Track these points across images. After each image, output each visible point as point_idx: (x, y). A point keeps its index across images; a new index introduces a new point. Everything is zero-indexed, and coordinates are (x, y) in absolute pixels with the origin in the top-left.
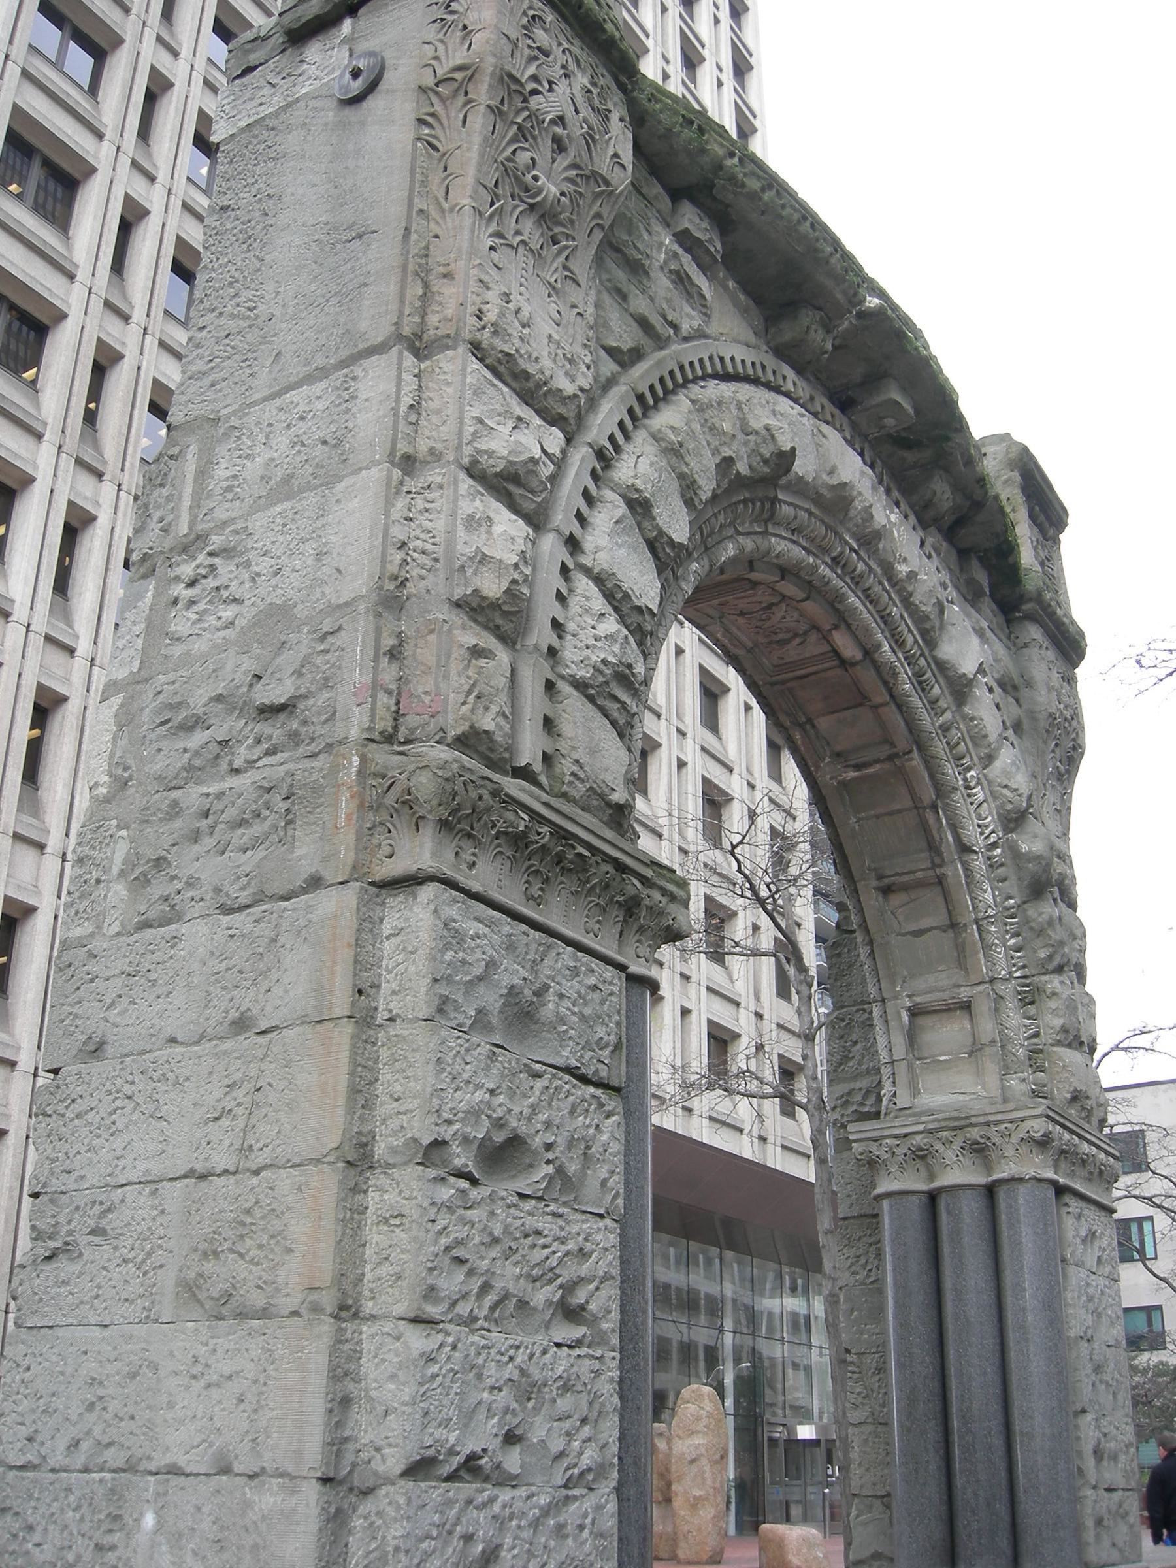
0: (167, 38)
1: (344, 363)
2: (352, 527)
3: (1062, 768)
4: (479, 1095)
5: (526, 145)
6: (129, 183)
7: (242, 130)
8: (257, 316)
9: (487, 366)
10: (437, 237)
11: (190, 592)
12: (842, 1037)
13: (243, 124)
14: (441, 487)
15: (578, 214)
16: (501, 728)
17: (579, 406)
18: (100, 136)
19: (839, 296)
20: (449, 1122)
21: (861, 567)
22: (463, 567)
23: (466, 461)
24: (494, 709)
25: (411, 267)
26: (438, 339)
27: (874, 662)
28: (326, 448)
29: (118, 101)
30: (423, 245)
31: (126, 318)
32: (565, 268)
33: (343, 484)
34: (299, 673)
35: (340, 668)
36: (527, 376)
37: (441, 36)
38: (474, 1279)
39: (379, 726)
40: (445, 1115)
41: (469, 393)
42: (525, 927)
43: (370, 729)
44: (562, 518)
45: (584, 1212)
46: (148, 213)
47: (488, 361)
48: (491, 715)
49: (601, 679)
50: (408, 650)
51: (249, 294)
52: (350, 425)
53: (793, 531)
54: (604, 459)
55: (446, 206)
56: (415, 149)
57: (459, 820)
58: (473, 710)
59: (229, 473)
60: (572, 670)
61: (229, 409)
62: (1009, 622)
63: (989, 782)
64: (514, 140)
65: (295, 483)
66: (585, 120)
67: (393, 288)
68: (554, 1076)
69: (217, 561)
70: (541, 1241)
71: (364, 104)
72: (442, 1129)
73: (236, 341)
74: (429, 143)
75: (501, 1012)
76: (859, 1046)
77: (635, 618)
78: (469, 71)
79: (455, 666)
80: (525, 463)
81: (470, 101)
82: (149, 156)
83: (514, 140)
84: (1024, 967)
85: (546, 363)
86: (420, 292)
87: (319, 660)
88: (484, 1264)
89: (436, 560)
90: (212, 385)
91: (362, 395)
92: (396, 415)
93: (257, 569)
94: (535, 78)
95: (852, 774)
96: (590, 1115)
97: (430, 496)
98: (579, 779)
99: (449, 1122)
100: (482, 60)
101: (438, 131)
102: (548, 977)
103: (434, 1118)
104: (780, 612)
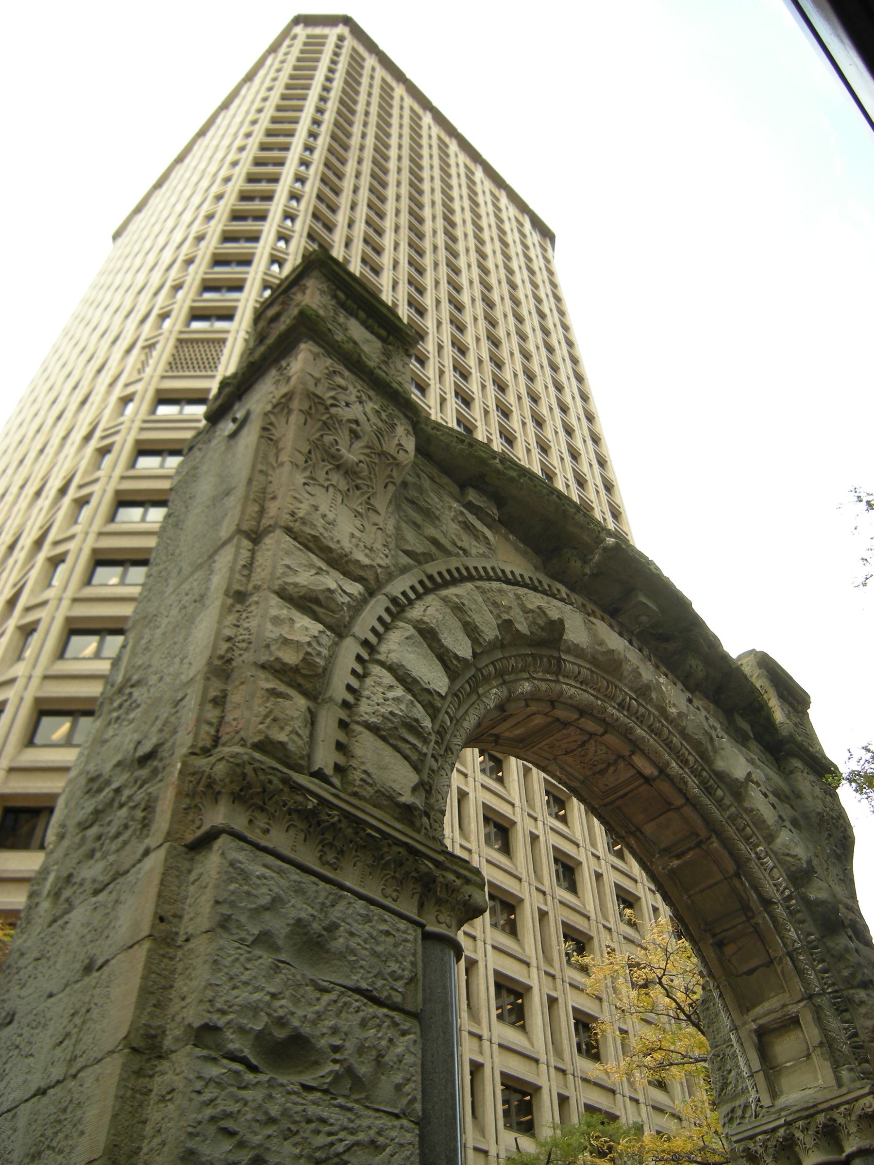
3: (838, 851)
4: (257, 996)
9: (300, 543)
12: (720, 1069)
19: (586, 538)
20: (223, 1012)
21: (642, 710)
27: (668, 776)
32: (367, 503)
36: (330, 550)
38: (245, 1151)
39: (201, 744)
40: (219, 1005)
42: (314, 879)
45: (378, 1110)
53: (581, 683)
57: (249, 792)
58: (268, 727)
62: (777, 760)
63: (775, 853)
68: (342, 993)
70: (327, 1129)
72: (215, 1017)
75: (286, 937)
76: (733, 1073)
77: (426, 697)
79: (257, 701)
80: (323, 591)
84: (833, 984)
88: (257, 1139)
89: (250, 643)
95: (676, 863)
96: (384, 1030)
98: (367, 783)
99: (223, 1012)
102: (339, 918)
103: (207, 1006)
104: (592, 747)
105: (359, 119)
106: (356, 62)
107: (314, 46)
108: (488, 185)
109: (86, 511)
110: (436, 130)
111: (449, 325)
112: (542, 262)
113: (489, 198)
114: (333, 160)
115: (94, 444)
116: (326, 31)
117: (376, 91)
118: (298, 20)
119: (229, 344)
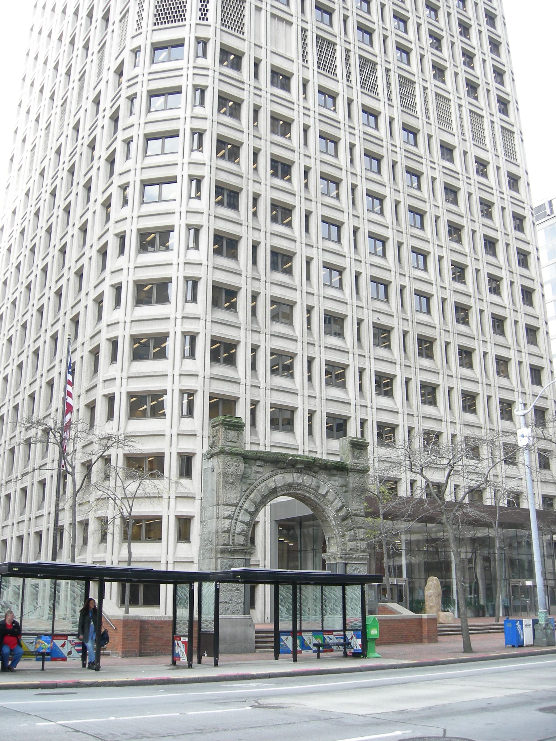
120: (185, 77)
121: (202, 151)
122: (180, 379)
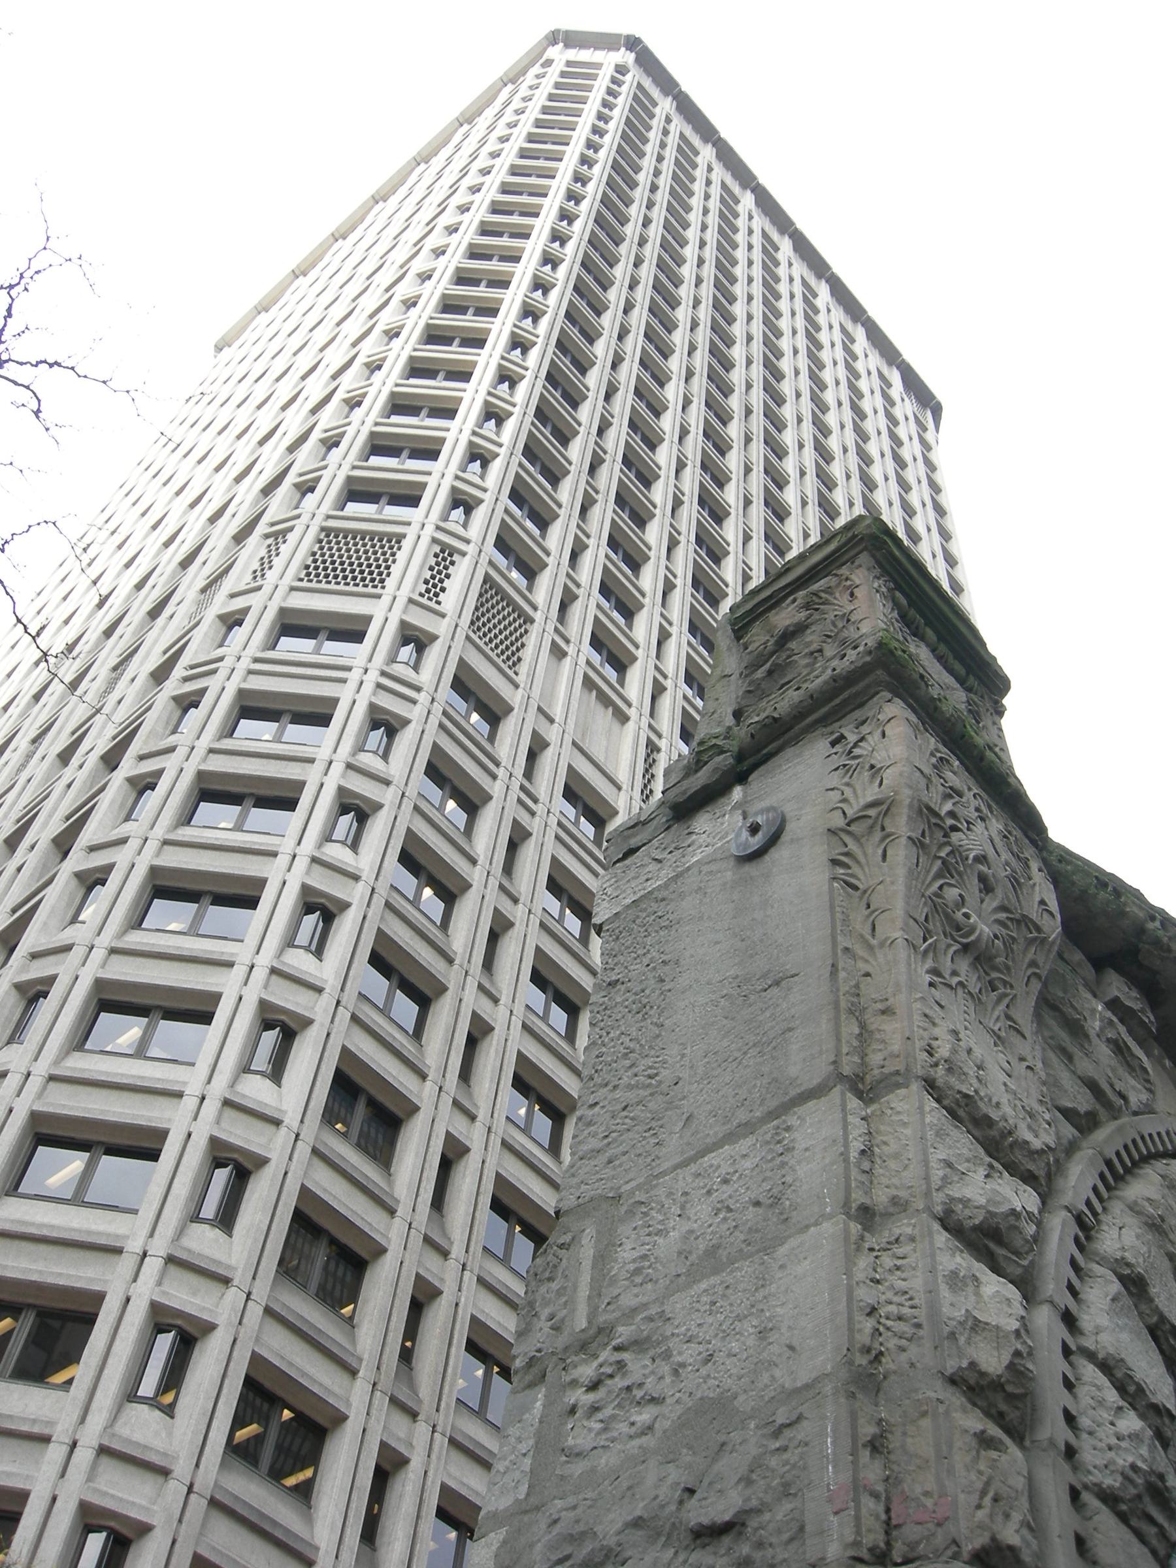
0: (487, 986)
1: (773, 1115)
2: (807, 1294)
5: (953, 882)
6: (449, 1121)
7: (628, 907)
8: (660, 1082)
10: (867, 975)
11: (591, 1397)
13: (628, 901)
14: (912, 1239)
15: (1013, 960)
16: (1028, 1545)
17: (1048, 1164)
18: (423, 1077)
22: (953, 1334)
23: (939, 1209)
24: (1016, 1517)
25: (843, 1005)
26: (885, 1078)
28: (760, 1211)
29: (441, 1042)
30: (853, 983)
31: (445, 1254)
32: (1008, 1017)
33: (786, 1246)
34: (747, 1481)
35: (805, 1468)
37: (846, 779)
39: (868, 1540)
41: (930, 1134)
43: (856, 1544)
44: (1052, 1285)
46: (468, 1150)
47: (946, 1102)
48: (1013, 1524)
49: (1133, 1491)
50: (894, 1441)
51: (649, 1062)
52: (789, 1179)
54: (1086, 1227)
55: (874, 942)
56: (831, 890)
59: (636, 1254)
60: (1096, 1477)
61: (633, 1184)
64: (938, 875)
65: (723, 1254)
66: (1007, 864)
67: (825, 1025)
69: (626, 1356)
71: (767, 858)
73: (637, 1111)
74: (846, 882)
78: (884, 806)
79: (960, 1459)
81: (889, 835)
82: (470, 1095)
83: (938, 875)
85: (1007, 1110)
86: (857, 1031)
87: (773, 1462)
89: (918, 1326)
90: (610, 1162)
91: (801, 1145)
92: (846, 1161)
93: (680, 1359)
94: (952, 814)
97: (900, 1251)
100: (896, 793)
101: (855, 869)
105: (640, 194)
106: (642, 106)
107: (575, 80)
108: (838, 315)
109: (152, 799)
110: (760, 222)
111: (763, 543)
112: (917, 448)
113: (837, 336)
114: (596, 257)
115: (173, 686)
116: (597, 56)
117: (670, 153)
118: (554, 38)
119: (407, 544)
120: (239, 971)
121: (169, 1410)
122: (94, 1467)
